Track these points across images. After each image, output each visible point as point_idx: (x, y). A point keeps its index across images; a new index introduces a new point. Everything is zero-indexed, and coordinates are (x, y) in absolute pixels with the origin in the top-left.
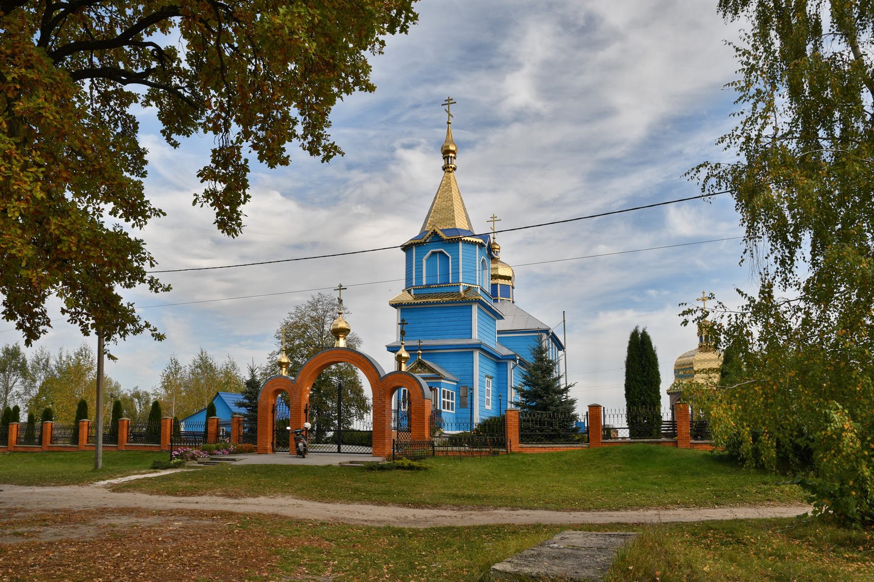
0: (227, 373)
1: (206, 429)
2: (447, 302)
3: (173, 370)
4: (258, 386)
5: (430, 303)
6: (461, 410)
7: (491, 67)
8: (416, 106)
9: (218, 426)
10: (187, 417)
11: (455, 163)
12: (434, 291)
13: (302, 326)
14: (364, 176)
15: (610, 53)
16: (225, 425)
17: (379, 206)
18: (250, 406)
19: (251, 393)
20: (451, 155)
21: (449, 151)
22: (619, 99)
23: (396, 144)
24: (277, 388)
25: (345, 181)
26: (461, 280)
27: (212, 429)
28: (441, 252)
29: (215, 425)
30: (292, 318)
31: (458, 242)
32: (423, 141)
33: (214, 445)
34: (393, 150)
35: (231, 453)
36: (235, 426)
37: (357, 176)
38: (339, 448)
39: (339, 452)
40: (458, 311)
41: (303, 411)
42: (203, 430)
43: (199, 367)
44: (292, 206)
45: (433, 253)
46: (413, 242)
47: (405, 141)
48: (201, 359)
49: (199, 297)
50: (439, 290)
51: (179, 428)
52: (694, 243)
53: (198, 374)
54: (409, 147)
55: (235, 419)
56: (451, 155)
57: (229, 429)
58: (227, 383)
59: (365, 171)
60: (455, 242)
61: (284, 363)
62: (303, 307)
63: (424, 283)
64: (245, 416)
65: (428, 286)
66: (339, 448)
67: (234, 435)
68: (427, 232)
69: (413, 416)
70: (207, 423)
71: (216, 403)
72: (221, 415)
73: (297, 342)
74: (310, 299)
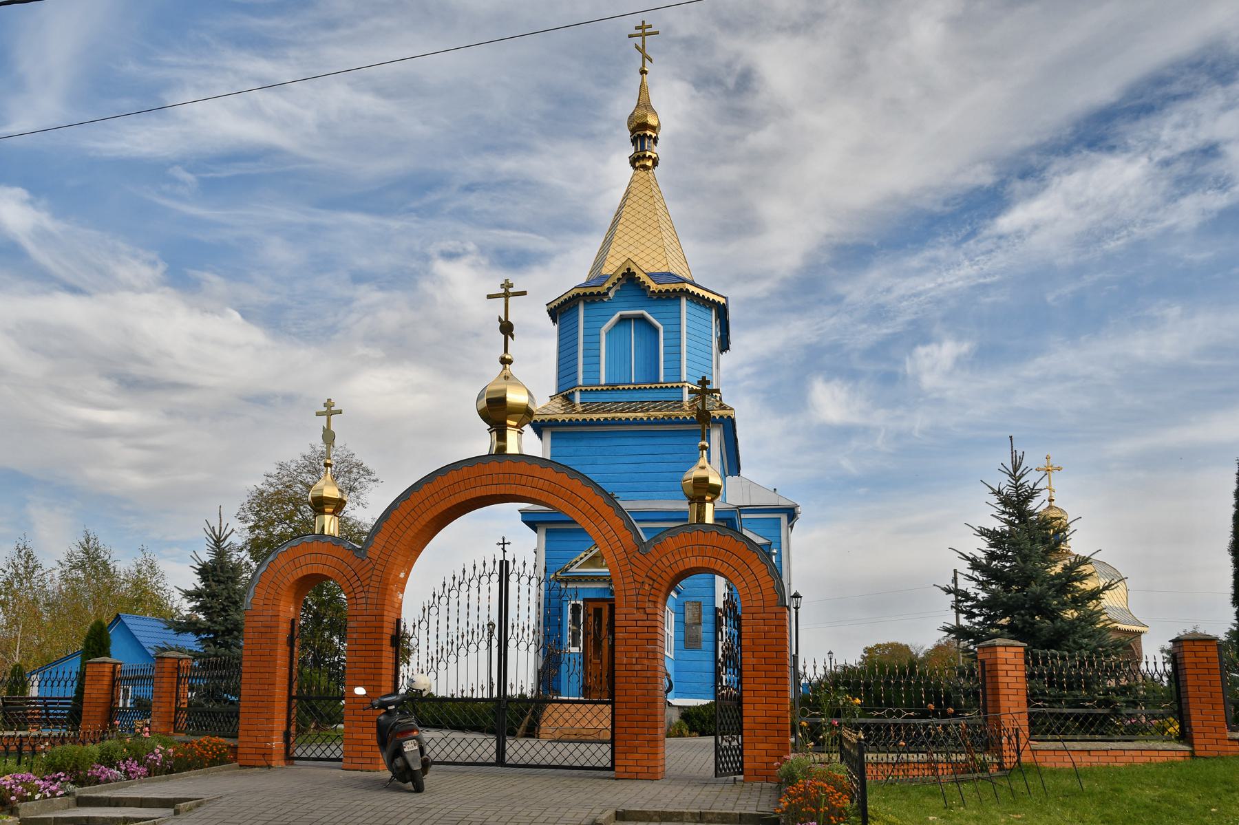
0: (138, 584)
1: (80, 691)
2: (657, 422)
3: (22, 570)
4: (234, 580)
5: (620, 422)
6: (690, 654)
7: (589, 136)
8: (470, 188)
9: (114, 683)
10: (47, 664)
11: (657, 150)
12: (626, 397)
13: (290, 501)
14: (376, 296)
15: (764, 138)
16: (135, 680)
17: (399, 348)
18: (208, 631)
19: (213, 595)
20: (649, 133)
21: (645, 126)
22: (773, 208)
23: (433, 250)
24: (300, 573)
25: (348, 302)
26: (684, 378)
27: (96, 691)
28: (641, 319)
29: (106, 681)
30: (271, 485)
31: (679, 298)
32: (471, 247)
33: (94, 749)
34: (427, 258)
35: (154, 771)
36: (167, 683)
37: (368, 295)
38: (501, 751)
39: (501, 761)
40: (679, 440)
41: (387, 641)
42: (70, 692)
43: (81, 566)
44: (256, 335)
45: (624, 320)
46: (581, 291)
47: (450, 245)
48: (86, 551)
49: (94, 473)
50: (637, 396)
51: (25, 685)
52: (844, 433)
53: (77, 580)
54: (450, 256)
55: (168, 665)
56: (649, 133)
57: (145, 692)
58: (139, 600)
59: (381, 289)
60: (672, 297)
61: (330, 500)
62: (293, 466)
63: (603, 381)
64: (196, 656)
65: (612, 388)
66: (501, 751)
67: (161, 708)
68: (607, 277)
69: (749, 659)
70: (82, 676)
71: (115, 636)
72: (120, 654)
73: (278, 530)
74: (308, 452)
